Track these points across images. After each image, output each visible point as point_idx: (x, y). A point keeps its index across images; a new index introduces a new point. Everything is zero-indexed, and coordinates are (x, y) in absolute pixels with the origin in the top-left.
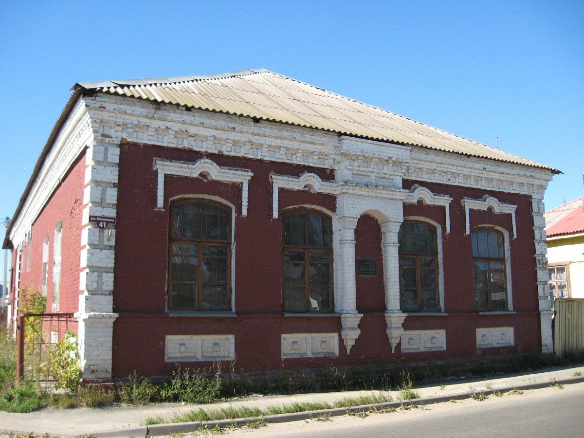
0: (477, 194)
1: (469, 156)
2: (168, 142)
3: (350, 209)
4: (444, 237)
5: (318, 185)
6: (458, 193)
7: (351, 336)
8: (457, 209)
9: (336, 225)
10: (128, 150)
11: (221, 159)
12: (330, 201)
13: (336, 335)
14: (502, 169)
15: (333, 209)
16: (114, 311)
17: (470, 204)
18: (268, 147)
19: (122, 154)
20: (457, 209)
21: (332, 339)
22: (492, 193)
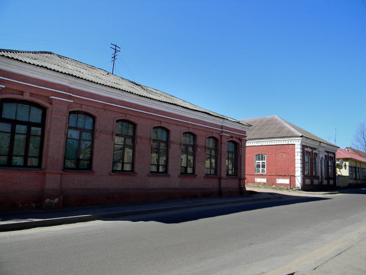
7: (321, 180)
9: (317, 159)
12: (316, 154)
21: (317, 181)
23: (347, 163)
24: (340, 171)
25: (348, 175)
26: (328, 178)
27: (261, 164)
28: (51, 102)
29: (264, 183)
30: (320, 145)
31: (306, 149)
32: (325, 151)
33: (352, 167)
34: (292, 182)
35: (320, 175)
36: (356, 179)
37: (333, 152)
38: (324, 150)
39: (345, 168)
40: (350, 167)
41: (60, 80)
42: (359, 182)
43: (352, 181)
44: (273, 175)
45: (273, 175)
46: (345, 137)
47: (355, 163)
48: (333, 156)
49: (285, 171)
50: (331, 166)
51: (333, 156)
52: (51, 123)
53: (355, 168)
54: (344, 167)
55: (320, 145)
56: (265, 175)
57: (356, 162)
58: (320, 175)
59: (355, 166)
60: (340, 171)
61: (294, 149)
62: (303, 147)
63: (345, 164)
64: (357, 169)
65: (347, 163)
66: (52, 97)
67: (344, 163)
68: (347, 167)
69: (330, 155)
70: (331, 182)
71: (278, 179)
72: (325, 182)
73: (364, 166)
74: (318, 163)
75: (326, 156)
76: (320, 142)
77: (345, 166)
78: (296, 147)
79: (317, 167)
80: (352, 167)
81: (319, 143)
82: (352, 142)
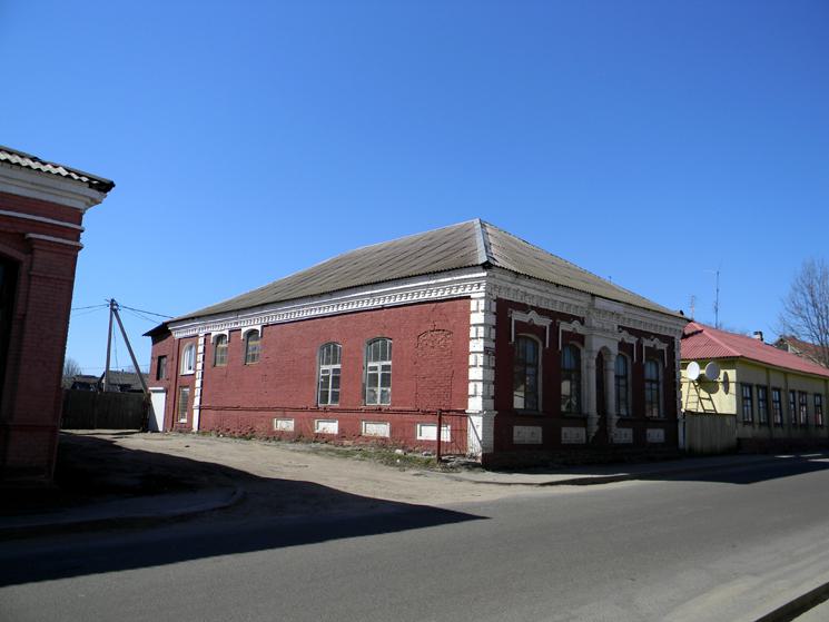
0: (524, 308)
1: (649, 310)
2: (517, 299)
3: (597, 343)
4: (544, 352)
5: (580, 330)
6: (556, 317)
7: (595, 428)
8: (554, 327)
9: (584, 355)
10: (499, 301)
11: (541, 312)
12: (581, 338)
13: (583, 430)
14: (664, 319)
15: (583, 344)
16: (495, 409)
17: (564, 326)
18: (559, 302)
19: (497, 306)
20: (554, 327)
21: (582, 431)
22: (656, 335)
23: (732, 374)
24: (710, 399)
25: (734, 412)
26: (638, 421)
27: (380, 372)
28: (29, 247)
29: (384, 439)
30: (592, 306)
31: (517, 316)
32: (622, 328)
33: (751, 387)
34: (460, 434)
35: (591, 407)
36: (767, 424)
37: (667, 333)
38: (615, 324)
39: (727, 391)
40: (741, 384)
41: (28, 188)
42: (779, 433)
43: (748, 432)
44: (407, 412)
45: (407, 412)
46: (734, 292)
47: (764, 373)
48: (664, 346)
49: (439, 396)
50: (657, 382)
51: (664, 346)
52: (27, 301)
53: (765, 388)
54: (721, 387)
55: (592, 306)
56: (387, 411)
57: (767, 369)
58: (591, 407)
59: (763, 382)
60: (710, 399)
61: (467, 313)
62: (501, 310)
63: (726, 374)
64: (775, 395)
65: (732, 374)
66: (32, 235)
67: (722, 372)
68: (732, 387)
69: (646, 343)
70: (656, 435)
71: (423, 424)
72: (623, 435)
73: (823, 388)
74: (588, 367)
75: (622, 345)
76: (593, 295)
77: (726, 382)
78: (473, 305)
79: (584, 383)
80: (751, 387)
81: (589, 299)
82: (782, 319)
